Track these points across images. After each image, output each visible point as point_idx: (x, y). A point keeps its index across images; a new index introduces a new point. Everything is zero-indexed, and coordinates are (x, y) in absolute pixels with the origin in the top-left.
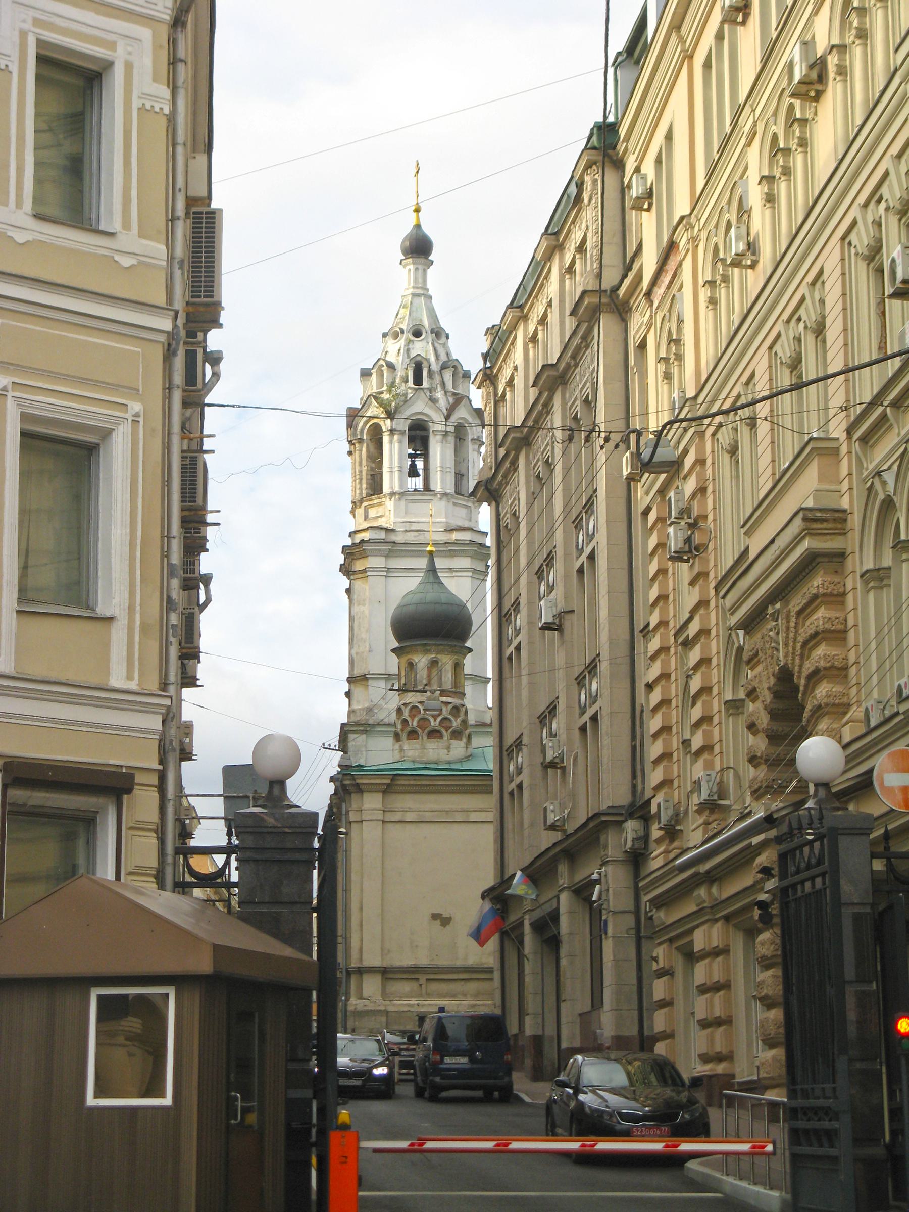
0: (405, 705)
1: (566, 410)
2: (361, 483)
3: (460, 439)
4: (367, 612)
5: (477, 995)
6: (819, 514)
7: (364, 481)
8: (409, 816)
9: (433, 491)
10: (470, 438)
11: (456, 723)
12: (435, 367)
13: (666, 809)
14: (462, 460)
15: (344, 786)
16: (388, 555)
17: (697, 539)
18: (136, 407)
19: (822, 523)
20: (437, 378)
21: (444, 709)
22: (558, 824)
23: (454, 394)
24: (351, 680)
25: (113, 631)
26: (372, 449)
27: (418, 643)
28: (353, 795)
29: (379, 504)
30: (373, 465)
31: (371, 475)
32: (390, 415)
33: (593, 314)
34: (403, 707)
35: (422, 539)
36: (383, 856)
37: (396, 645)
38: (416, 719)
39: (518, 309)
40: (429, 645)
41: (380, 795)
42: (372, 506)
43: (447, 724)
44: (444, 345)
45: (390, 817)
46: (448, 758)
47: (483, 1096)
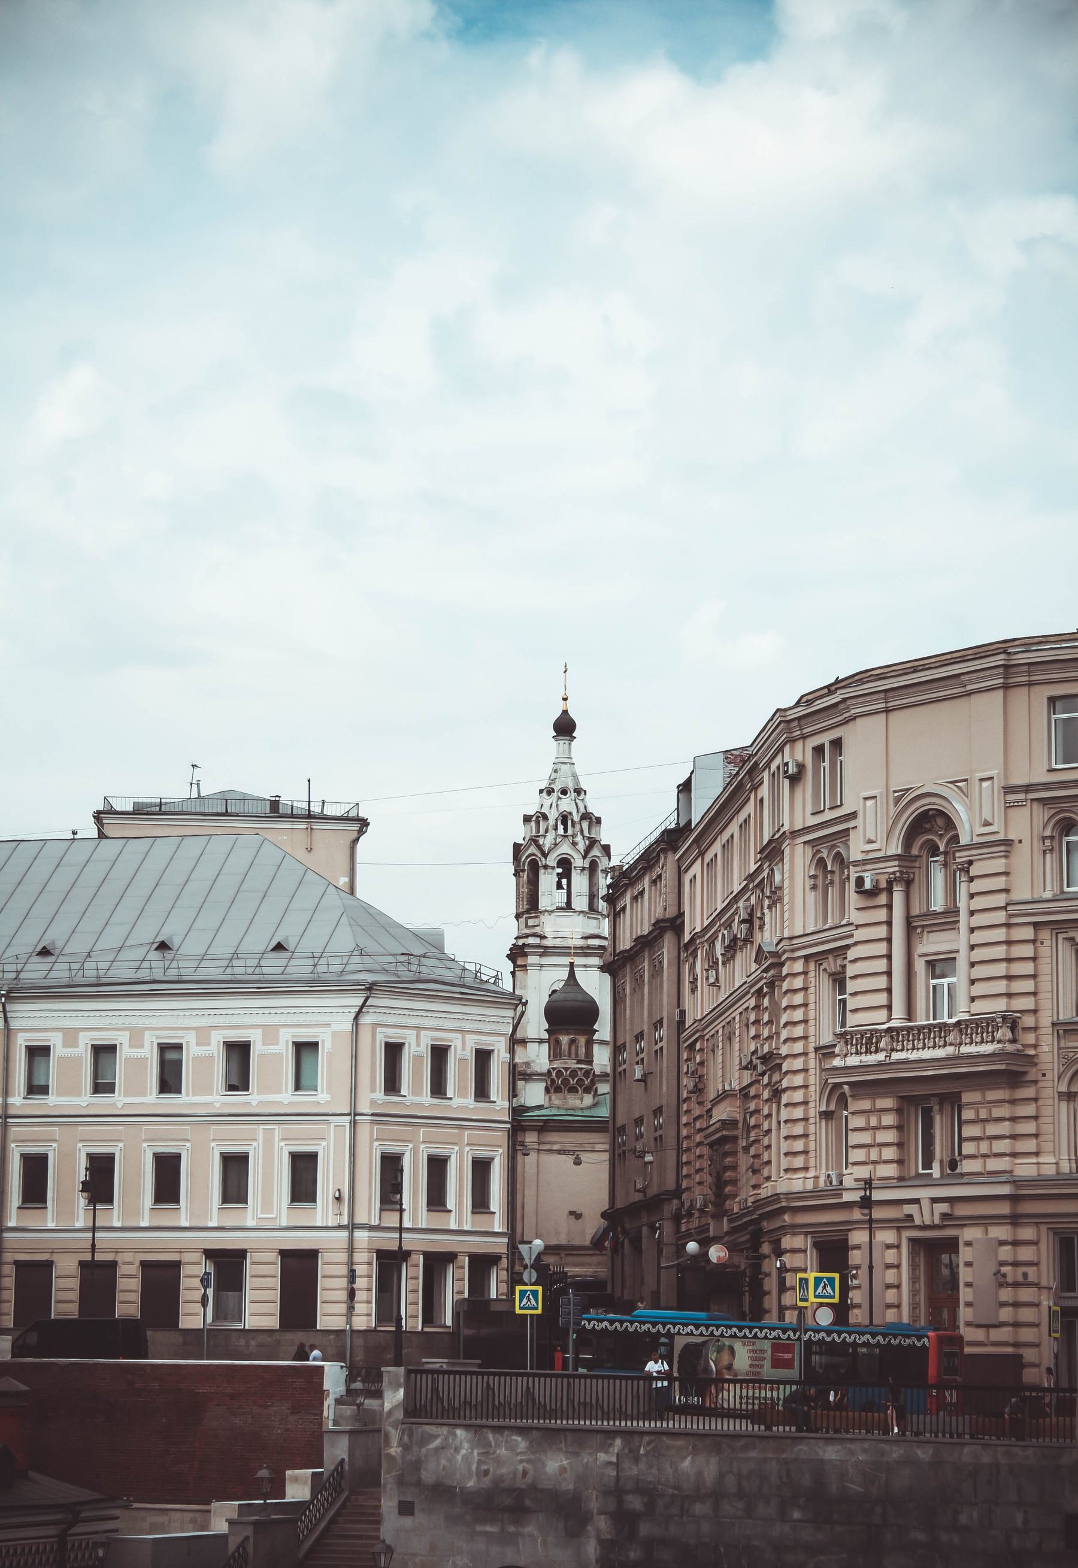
0: (554, 1069)
2: (523, 900)
5: (598, 1264)
10: (600, 869)
12: (576, 818)
16: (541, 955)
17: (700, 1086)
18: (501, 1151)
21: (579, 1073)
23: (589, 838)
26: (531, 875)
29: (536, 917)
34: (552, 1070)
35: (565, 943)
36: (538, 1173)
40: (569, 1029)
46: (582, 1106)
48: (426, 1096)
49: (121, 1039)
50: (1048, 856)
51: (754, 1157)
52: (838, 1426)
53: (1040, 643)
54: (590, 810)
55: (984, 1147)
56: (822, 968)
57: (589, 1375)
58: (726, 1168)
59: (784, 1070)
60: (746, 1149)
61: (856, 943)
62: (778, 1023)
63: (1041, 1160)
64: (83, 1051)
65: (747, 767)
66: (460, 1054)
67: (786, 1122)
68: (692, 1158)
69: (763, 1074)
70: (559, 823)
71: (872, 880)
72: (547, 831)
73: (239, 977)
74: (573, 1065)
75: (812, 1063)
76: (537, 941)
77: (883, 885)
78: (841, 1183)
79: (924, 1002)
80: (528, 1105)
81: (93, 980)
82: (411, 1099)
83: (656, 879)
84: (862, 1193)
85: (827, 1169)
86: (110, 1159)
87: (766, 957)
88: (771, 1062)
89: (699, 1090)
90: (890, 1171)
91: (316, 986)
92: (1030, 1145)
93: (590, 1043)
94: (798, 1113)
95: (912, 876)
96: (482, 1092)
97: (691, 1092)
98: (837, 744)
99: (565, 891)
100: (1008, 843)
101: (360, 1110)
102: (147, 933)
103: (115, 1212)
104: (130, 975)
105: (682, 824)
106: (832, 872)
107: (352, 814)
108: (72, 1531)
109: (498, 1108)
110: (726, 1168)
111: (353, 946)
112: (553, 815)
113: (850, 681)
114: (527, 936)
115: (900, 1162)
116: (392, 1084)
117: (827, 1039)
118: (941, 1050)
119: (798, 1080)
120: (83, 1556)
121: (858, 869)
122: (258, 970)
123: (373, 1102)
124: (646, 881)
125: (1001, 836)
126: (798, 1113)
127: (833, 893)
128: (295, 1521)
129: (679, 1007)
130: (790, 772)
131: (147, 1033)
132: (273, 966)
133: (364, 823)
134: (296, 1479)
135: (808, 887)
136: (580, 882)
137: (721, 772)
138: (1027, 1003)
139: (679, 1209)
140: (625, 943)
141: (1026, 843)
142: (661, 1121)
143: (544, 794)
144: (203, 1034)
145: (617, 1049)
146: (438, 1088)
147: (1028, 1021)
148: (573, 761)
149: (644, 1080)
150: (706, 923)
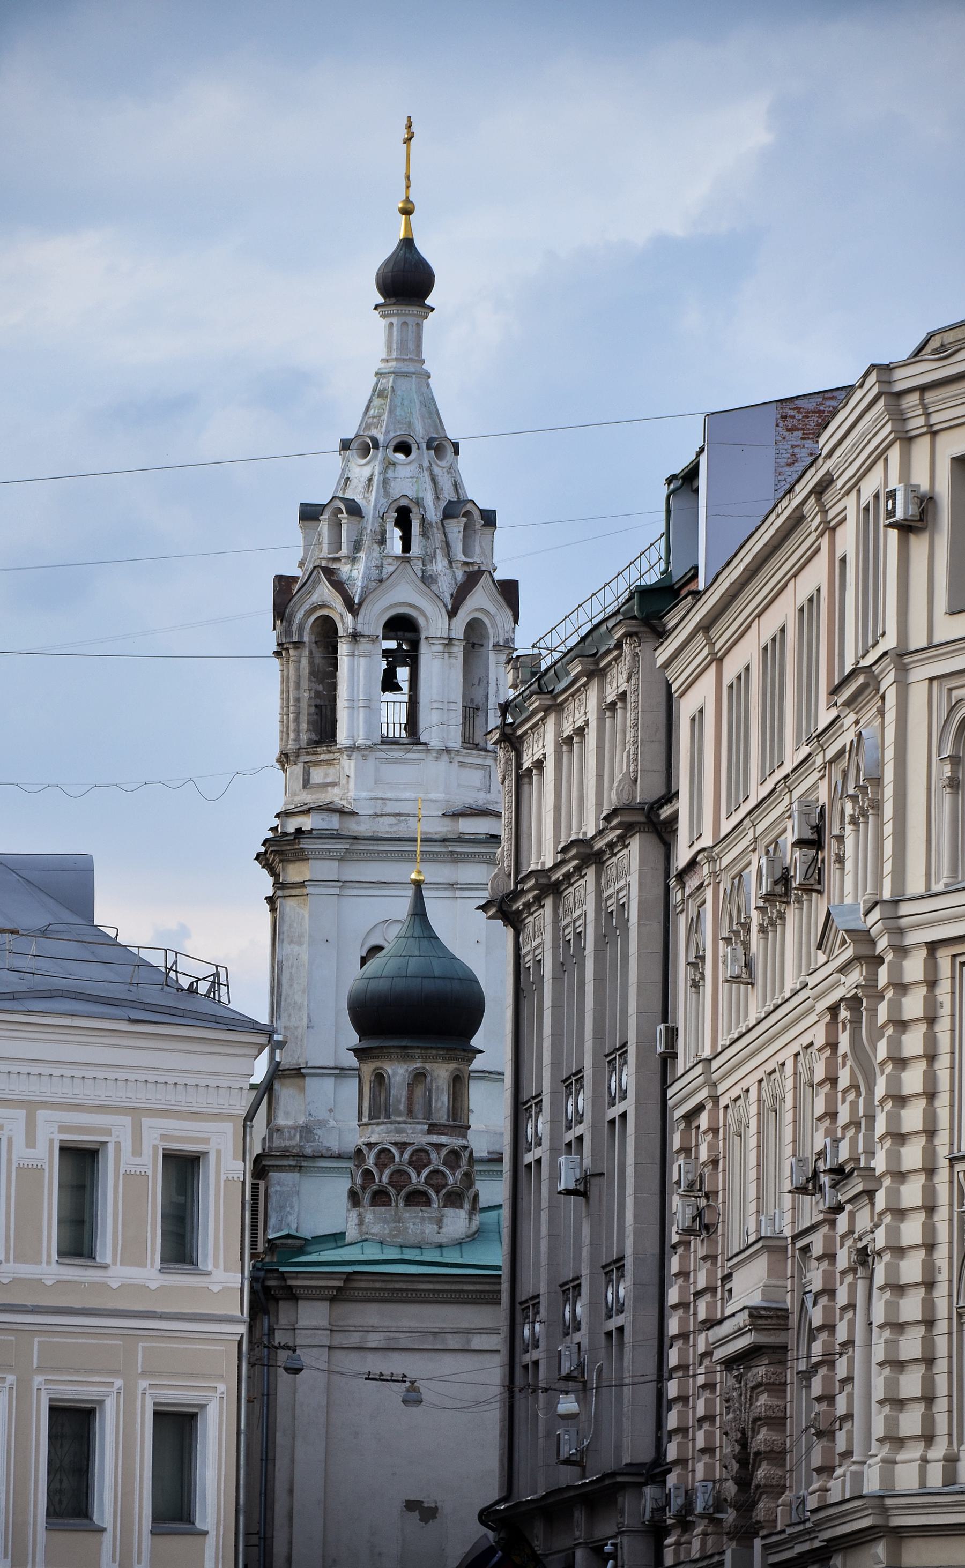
0: (370, 1145)
1: (601, 901)
3: (473, 645)
4: (305, 957)
6: (763, 1312)
7: (304, 718)
8: (374, 1340)
9: (426, 744)
11: (453, 1179)
12: (434, 515)
13: (676, 1497)
14: (476, 682)
15: (267, 1289)
18: (222, 1387)
19: (766, 1320)
20: (438, 536)
21: (434, 1155)
22: (574, 1458)
25: (207, 1539)
26: (318, 657)
27: (391, 1044)
28: (281, 1303)
29: (330, 762)
30: (320, 688)
31: (316, 706)
32: (352, 607)
35: (402, 830)
38: (387, 1172)
39: (549, 696)
40: (411, 1048)
41: (328, 1303)
42: (318, 763)
43: (436, 1180)
44: (452, 470)
45: (339, 1340)
46: (438, 1239)
48: (49, 1263)
60: (807, 1376)
66: (128, 1162)
72: (357, 546)
74: (418, 1135)
76: (334, 822)
80: (307, 1233)
83: (613, 704)
87: (844, 942)
93: (458, 1083)
97: (688, 1231)
99: (405, 698)
109: (216, 1288)
129: (665, 1020)
137: (772, 451)
139: (660, 1510)
142: (622, 1292)
149: (580, 1192)
150: (726, 827)
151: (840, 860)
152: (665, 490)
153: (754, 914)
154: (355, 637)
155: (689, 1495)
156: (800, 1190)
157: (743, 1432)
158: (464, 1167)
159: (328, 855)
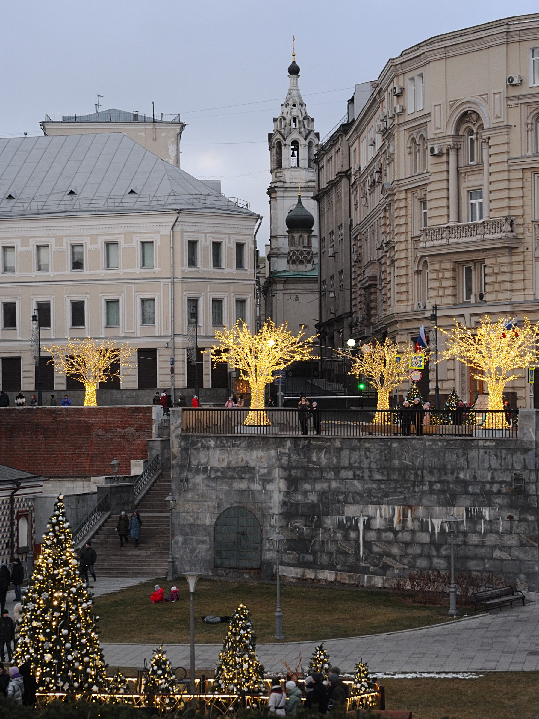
12: (301, 119)
17: (360, 259)
18: (251, 295)
20: (302, 123)
24: (272, 237)
29: (281, 172)
33: (341, 177)
37: (288, 229)
45: (285, 292)
46: (306, 270)
47: (142, 462)
49: (120, 239)
50: (530, 133)
51: (384, 295)
52: (396, 432)
53: (526, 19)
54: (308, 114)
55: (497, 287)
56: (414, 196)
57: (100, 409)
58: (371, 301)
59: (396, 250)
60: (381, 291)
61: (431, 183)
62: (393, 225)
63: (526, 293)
64: (101, 246)
65: (377, 90)
67: (397, 276)
68: (357, 296)
69: (387, 252)
70: (292, 122)
71: (439, 149)
73: (111, 208)
74: (301, 248)
75: (410, 246)
76: (282, 184)
77: (445, 151)
78: (425, 307)
79: (466, 212)
80: (279, 270)
81: (36, 212)
82: (202, 270)
84: (431, 313)
85: (418, 301)
86: (48, 304)
88: (389, 245)
89: (359, 261)
90: (450, 301)
91: (151, 211)
92: (520, 286)
93: (309, 237)
94: (403, 272)
95: (459, 146)
96: (240, 264)
98: (421, 76)
100: (508, 126)
101: (176, 276)
102: (64, 186)
103: (52, 331)
104: (55, 209)
105: (350, 121)
106: (419, 145)
107: (177, 120)
108: (17, 493)
110: (371, 301)
111: (171, 190)
112: (289, 118)
113: (427, 42)
114: (276, 182)
115: (454, 296)
116: (192, 262)
117: (417, 233)
118: (474, 237)
119: (403, 255)
120: (20, 506)
121: (432, 143)
122: (121, 205)
123: (182, 272)
124: (333, 151)
125: (505, 124)
126: (403, 272)
127: (419, 155)
128: (133, 486)
129: (350, 217)
130: (397, 93)
131: (64, 238)
132: (129, 201)
133: (183, 125)
134: (136, 465)
135: (407, 154)
136: (303, 152)
138: (519, 212)
140: (324, 185)
141: (518, 127)
143: (284, 106)
144: (93, 238)
145: (321, 240)
146: (217, 263)
147: (520, 221)
148: (299, 88)
151: (386, 175)
152: (347, 103)
153: (368, 191)
154: (285, 145)
155: (357, 318)
156: (379, 249)
157: (368, 304)
158: (311, 255)
159: (280, 191)
